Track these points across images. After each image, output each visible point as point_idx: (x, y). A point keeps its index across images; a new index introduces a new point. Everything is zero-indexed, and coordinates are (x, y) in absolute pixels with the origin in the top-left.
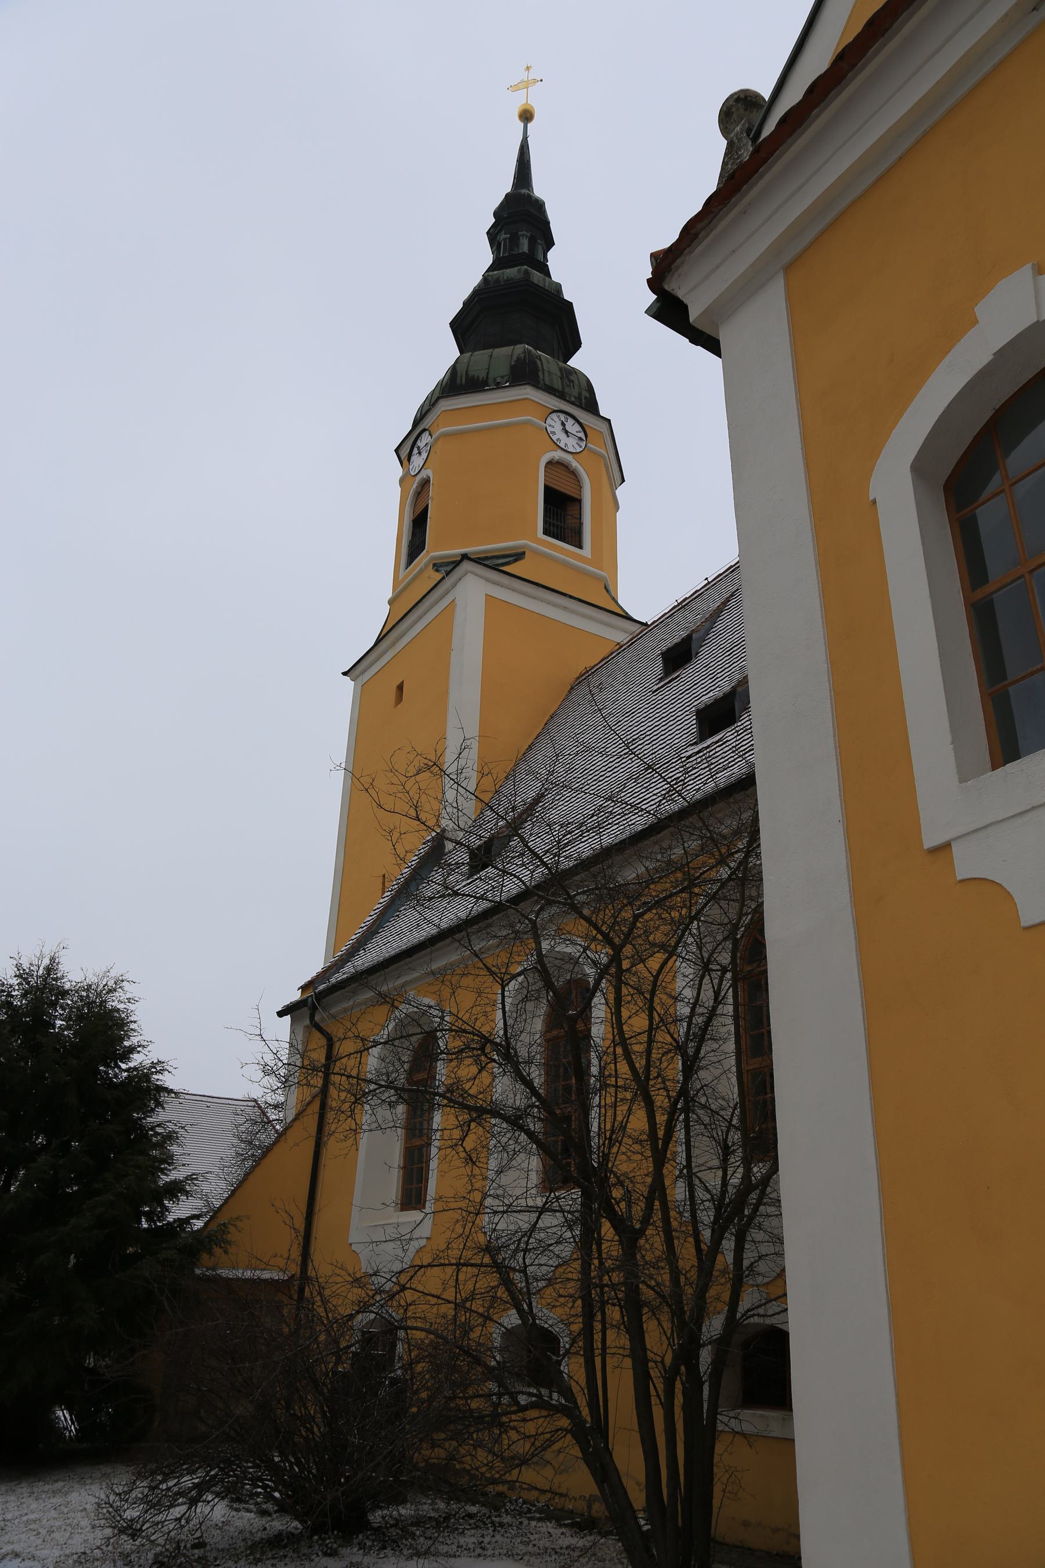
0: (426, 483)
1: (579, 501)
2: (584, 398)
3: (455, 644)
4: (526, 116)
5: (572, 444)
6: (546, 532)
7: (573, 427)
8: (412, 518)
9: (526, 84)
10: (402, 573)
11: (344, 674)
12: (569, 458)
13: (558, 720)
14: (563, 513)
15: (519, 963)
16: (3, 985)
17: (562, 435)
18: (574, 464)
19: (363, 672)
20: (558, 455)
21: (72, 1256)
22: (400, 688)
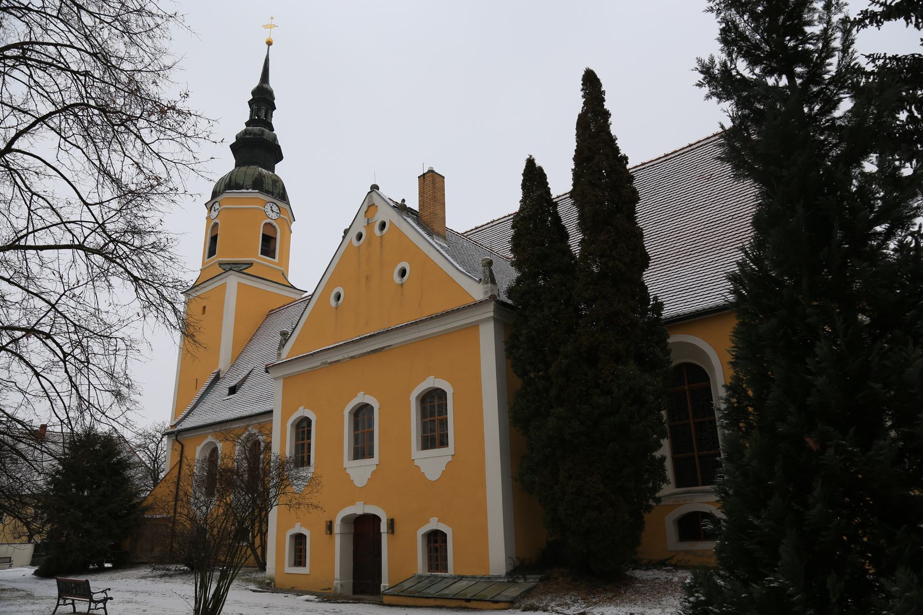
0: (216, 224)
1: (275, 239)
2: (279, 193)
3: (226, 300)
4: (269, 43)
5: (274, 216)
6: (262, 254)
7: (275, 208)
9: (271, 26)
12: (272, 221)
13: (261, 331)
14: (269, 245)
15: (160, 514)
17: (270, 212)
18: (275, 224)
20: (268, 221)
21: (919, 116)
22: (204, 307)
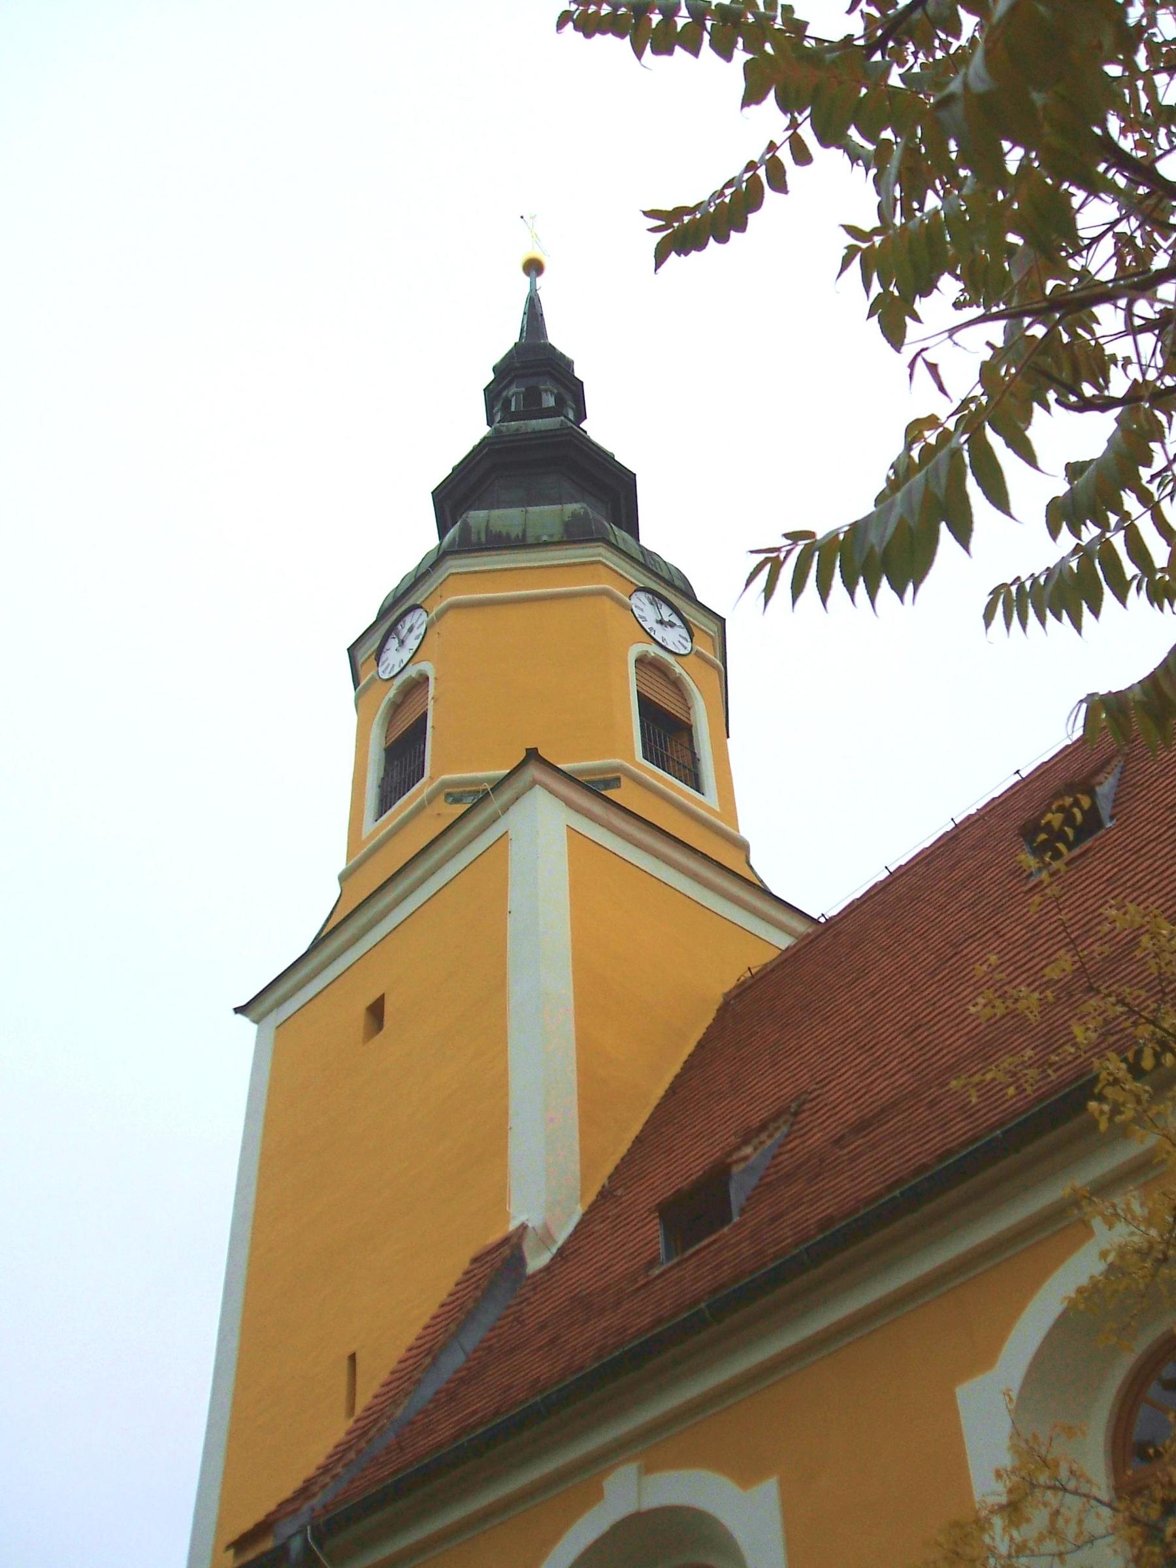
4: (534, 267)
8: (384, 746)
10: (369, 826)
11: (237, 1010)
12: (670, 659)
14: (670, 735)
16: (1137, 1559)
19: (279, 1003)
20: (653, 650)
